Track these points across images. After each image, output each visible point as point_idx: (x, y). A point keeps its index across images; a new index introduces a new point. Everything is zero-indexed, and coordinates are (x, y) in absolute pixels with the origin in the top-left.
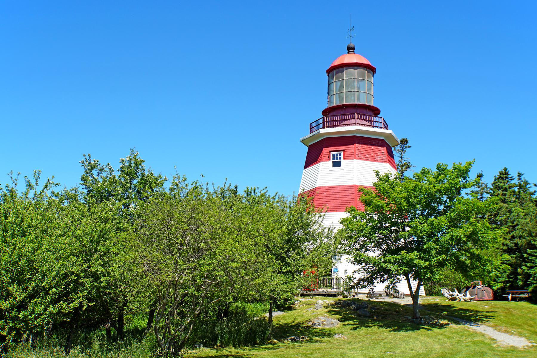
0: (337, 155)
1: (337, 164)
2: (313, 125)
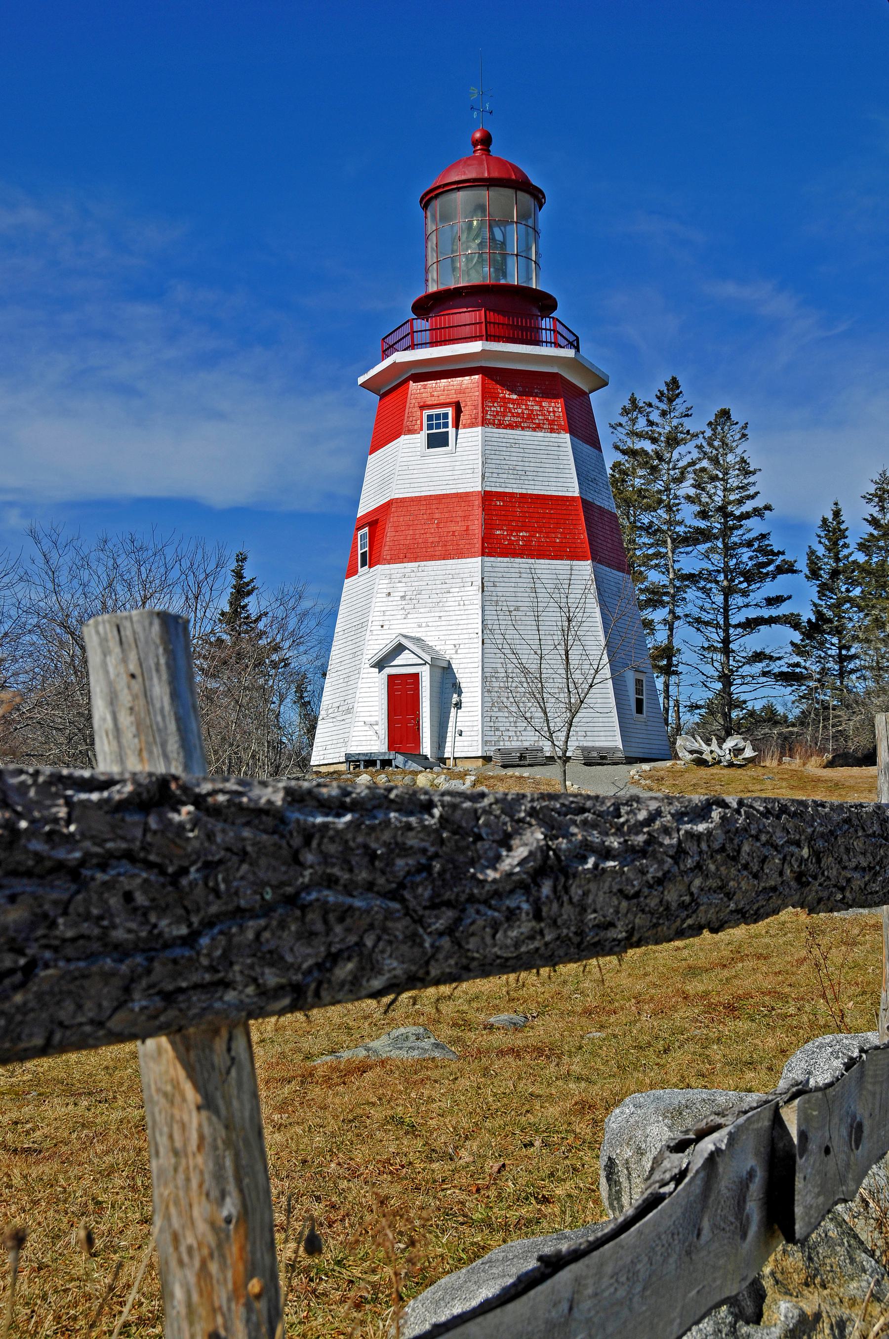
0: (438, 416)
1: (437, 441)
2: (391, 340)
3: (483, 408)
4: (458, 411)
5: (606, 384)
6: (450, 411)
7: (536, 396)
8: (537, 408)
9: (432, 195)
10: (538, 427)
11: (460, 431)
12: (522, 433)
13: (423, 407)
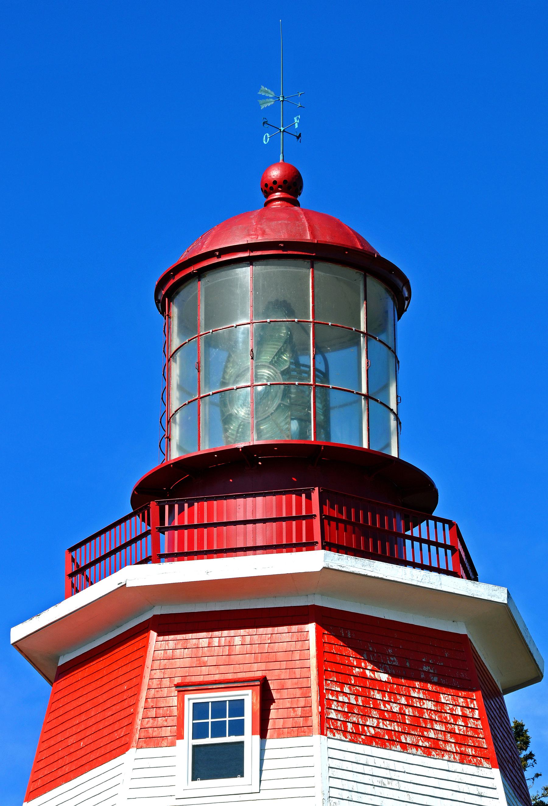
0: (219, 708)
1: (216, 763)
2: (83, 557)
3: (322, 696)
4: (266, 699)
5: (538, 678)
6: (249, 698)
7: (427, 680)
8: (429, 705)
9: (193, 269)
10: (434, 748)
11: (270, 743)
12: (403, 757)
13: (183, 688)
